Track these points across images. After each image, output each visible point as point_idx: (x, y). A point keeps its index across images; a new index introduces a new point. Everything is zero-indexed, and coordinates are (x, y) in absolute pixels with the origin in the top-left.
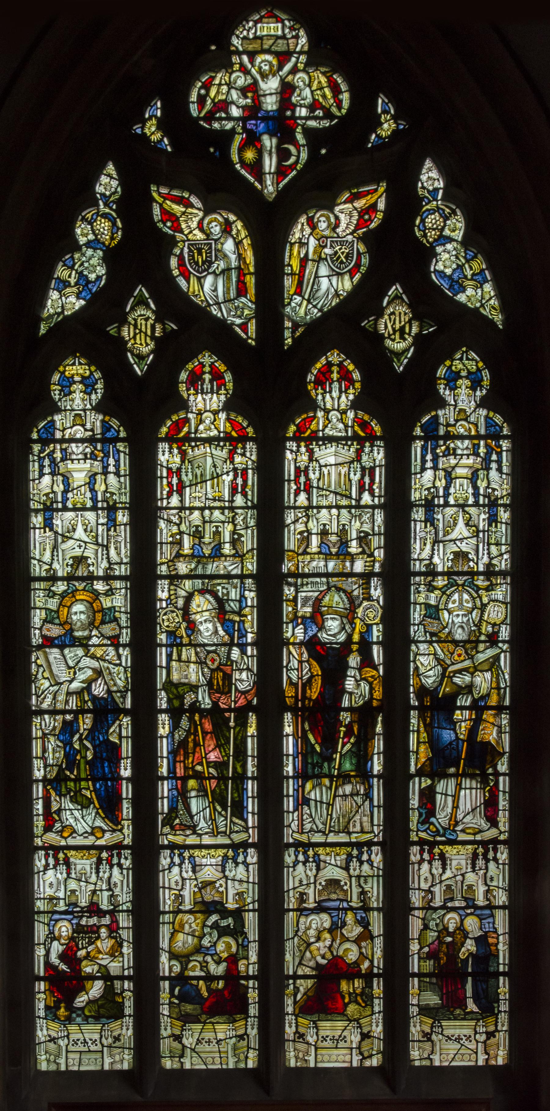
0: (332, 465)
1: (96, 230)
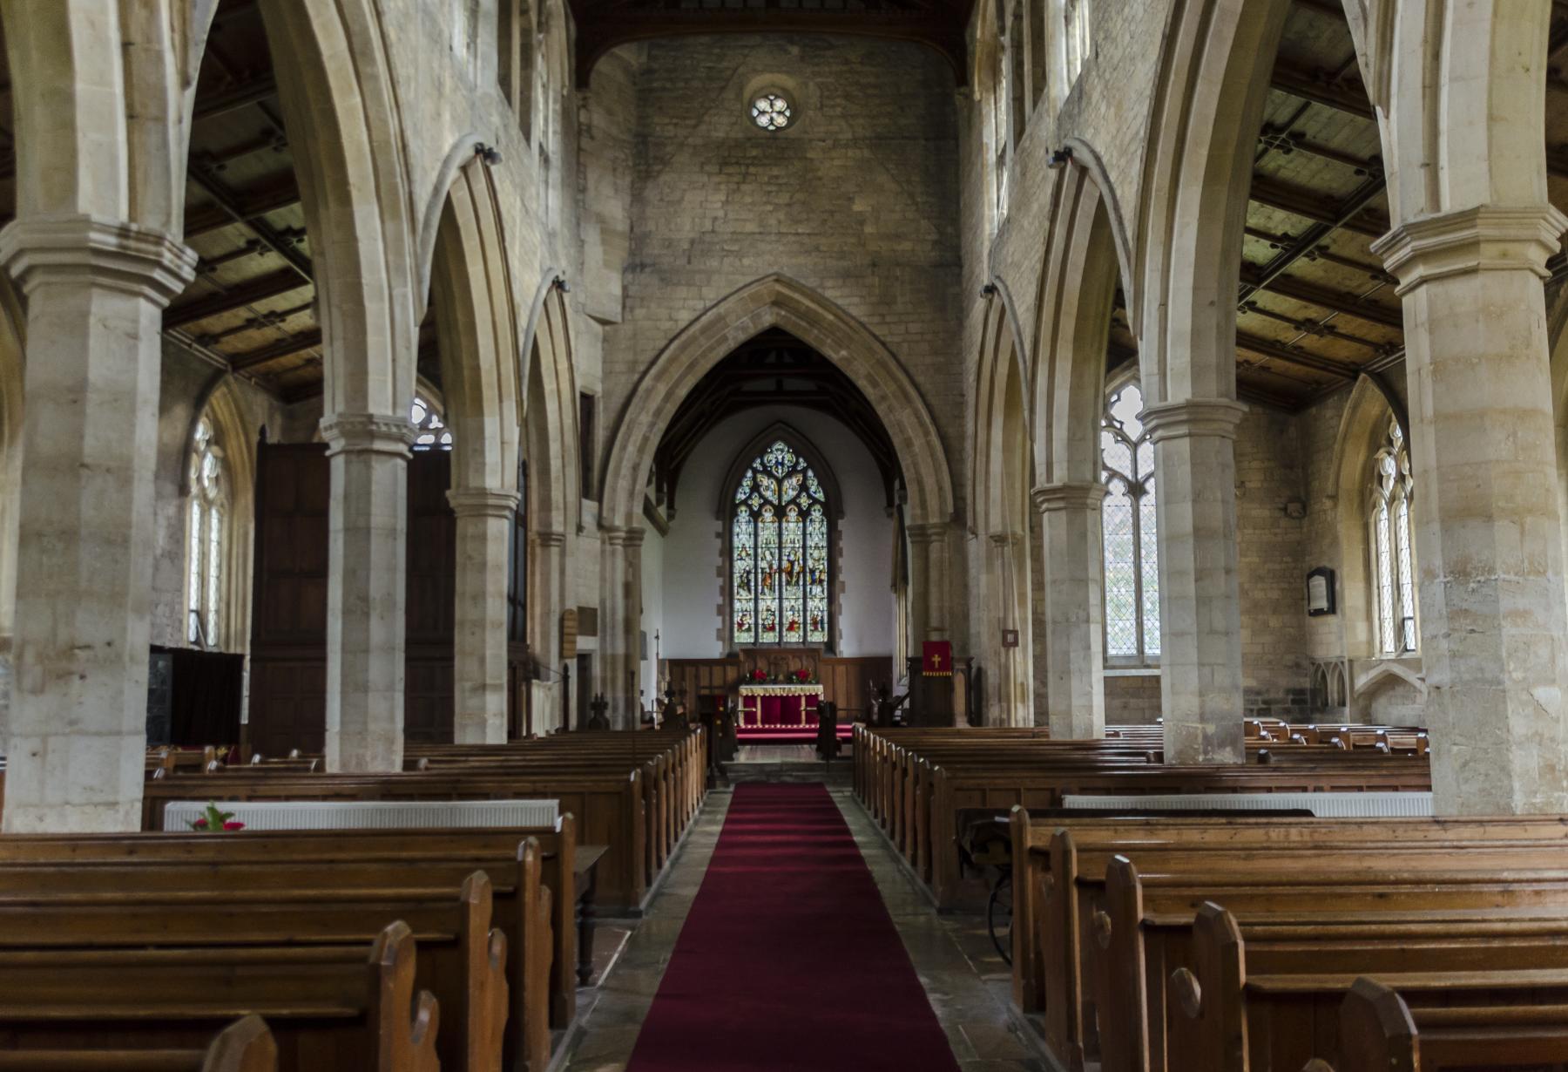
0: (792, 526)
1: (747, 483)
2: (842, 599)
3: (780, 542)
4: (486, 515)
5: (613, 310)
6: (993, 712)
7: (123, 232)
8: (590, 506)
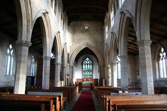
1: (84, 62)
2: (94, 73)
5: (71, 46)
6: (107, 84)
7: (26, 41)
8: (68, 64)
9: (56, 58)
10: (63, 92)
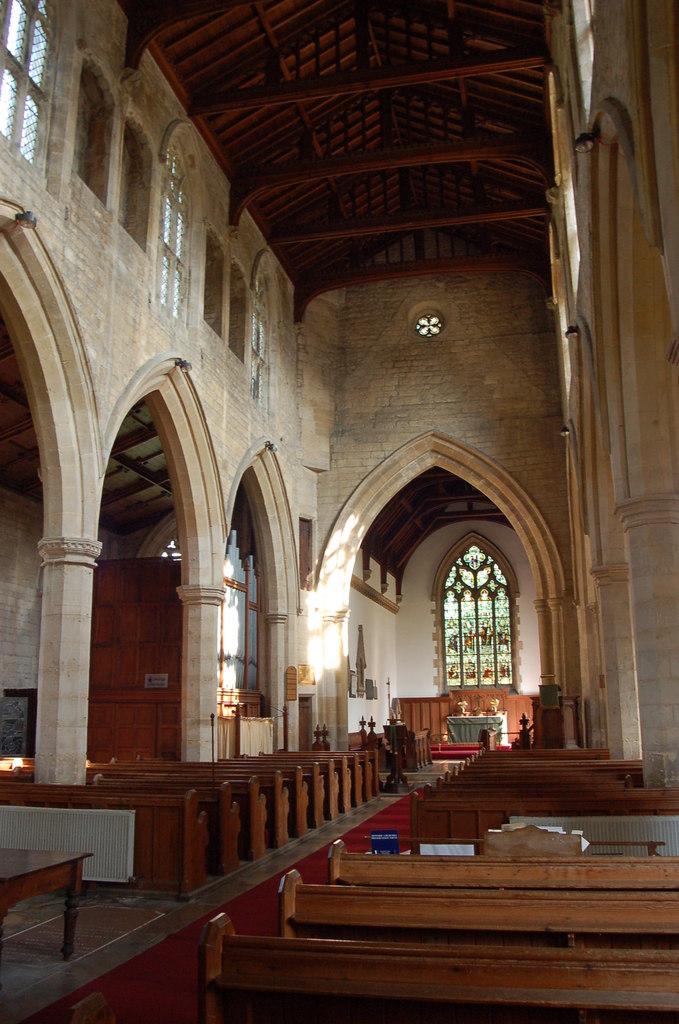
0: (485, 604)
1: (453, 574)
3: (477, 615)
4: (200, 604)
5: (323, 462)
9: (185, 555)
10: (134, 807)
